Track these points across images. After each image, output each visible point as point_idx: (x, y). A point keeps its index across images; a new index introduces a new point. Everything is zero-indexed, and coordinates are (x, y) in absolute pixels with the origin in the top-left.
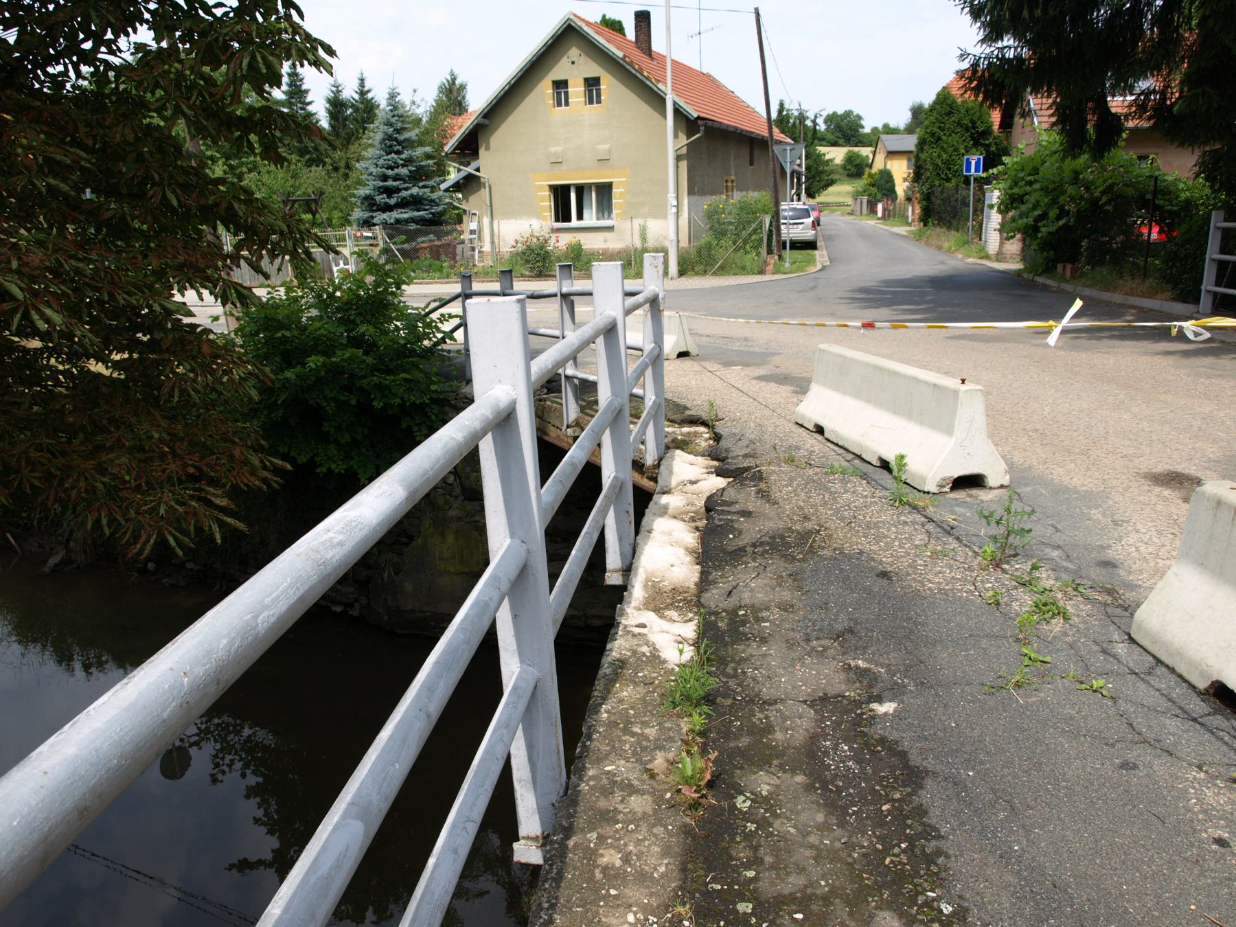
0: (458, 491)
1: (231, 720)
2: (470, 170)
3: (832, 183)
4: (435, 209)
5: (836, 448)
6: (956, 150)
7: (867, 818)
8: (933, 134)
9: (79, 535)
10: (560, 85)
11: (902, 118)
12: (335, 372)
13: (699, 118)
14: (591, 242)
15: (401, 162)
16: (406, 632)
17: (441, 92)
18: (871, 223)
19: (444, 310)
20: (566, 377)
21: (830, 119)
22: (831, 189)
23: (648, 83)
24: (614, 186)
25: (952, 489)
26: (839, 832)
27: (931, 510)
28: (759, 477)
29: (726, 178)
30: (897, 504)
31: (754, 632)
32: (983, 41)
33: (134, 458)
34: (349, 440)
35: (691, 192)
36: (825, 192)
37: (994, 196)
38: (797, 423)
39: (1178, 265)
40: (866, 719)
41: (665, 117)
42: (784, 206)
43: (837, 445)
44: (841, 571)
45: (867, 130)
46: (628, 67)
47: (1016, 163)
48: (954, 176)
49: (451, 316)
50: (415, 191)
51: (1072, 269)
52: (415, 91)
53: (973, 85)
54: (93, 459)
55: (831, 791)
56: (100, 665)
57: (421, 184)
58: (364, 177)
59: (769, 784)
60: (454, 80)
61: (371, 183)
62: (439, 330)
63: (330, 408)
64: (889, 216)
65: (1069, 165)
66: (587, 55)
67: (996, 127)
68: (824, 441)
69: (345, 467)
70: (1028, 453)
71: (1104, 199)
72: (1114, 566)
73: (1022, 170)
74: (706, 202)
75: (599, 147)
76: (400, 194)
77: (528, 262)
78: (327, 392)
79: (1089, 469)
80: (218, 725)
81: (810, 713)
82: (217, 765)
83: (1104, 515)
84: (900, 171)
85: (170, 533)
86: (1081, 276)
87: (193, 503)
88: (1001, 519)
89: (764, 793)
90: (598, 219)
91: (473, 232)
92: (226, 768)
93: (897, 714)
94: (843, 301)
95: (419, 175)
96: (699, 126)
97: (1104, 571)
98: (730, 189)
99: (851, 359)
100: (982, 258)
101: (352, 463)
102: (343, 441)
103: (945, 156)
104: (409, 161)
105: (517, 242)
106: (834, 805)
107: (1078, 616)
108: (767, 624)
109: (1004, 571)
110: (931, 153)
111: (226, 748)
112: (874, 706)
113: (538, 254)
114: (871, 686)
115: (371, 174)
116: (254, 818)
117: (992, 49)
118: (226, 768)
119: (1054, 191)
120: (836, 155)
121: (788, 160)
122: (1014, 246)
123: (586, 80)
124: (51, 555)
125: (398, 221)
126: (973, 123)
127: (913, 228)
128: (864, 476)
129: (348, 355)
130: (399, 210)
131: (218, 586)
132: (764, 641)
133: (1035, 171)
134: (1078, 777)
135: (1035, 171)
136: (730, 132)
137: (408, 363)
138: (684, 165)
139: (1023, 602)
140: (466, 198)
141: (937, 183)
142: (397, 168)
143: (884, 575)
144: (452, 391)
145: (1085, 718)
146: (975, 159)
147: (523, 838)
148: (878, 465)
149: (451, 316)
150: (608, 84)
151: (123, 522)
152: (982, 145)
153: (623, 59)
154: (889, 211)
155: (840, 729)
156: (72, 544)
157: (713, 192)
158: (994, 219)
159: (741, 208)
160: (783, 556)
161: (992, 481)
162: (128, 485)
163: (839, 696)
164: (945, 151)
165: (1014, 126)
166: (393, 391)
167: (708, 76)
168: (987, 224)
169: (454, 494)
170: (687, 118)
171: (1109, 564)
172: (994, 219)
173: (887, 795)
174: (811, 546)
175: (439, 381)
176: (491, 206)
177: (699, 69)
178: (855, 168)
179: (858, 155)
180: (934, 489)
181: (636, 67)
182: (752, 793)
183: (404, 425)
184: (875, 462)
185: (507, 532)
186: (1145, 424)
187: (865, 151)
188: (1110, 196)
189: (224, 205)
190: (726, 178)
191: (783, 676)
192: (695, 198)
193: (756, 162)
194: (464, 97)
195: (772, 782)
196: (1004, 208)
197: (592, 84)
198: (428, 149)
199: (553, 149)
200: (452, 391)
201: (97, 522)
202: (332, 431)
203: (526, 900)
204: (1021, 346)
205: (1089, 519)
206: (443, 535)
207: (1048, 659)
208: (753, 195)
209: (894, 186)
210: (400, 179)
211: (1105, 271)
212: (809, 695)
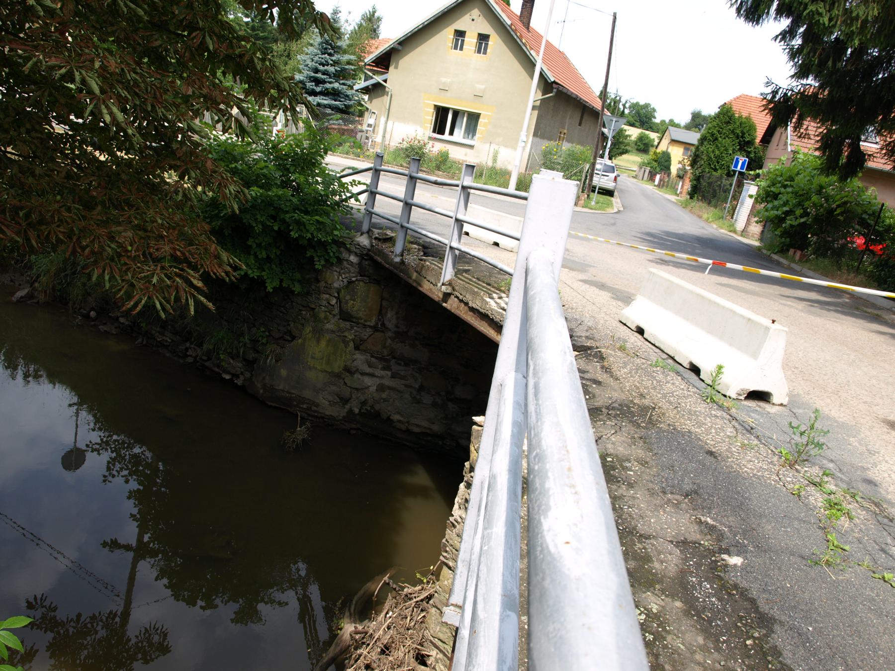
0: (336, 311)
1: (126, 438)
2: (378, 79)
3: (625, 152)
4: (347, 102)
5: (654, 348)
6: (726, 150)
7: (735, 647)
8: (713, 135)
9: (43, 279)
10: (460, 34)
11: (684, 118)
12: (269, 203)
13: (554, 82)
14: (456, 154)
15: (331, 62)
16: (274, 405)
17: (363, 19)
18: (649, 187)
19: (356, 177)
20: (451, 248)
21: (634, 106)
22: (625, 156)
23: (524, 48)
24: (481, 116)
25: (746, 398)
26: (716, 655)
27: (733, 411)
28: (602, 358)
29: (561, 130)
30: (708, 401)
31: (622, 476)
32: (792, 77)
33: (137, 234)
34: (265, 256)
35: (535, 134)
36: (620, 158)
37: (751, 189)
38: (621, 322)
39: (886, 270)
40: (721, 566)
41: (532, 76)
42: (599, 160)
43: (654, 345)
44: (679, 443)
45: (657, 120)
46: (512, 33)
47: (777, 170)
48: (720, 168)
49: (359, 183)
50: (336, 85)
51: (801, 255)
52: (350, 13)
53: (770, 107)
54: (106, 228)
55: (703, 619)
56: (37, 377)
57: (342, 82)
58: (301, 67)
59: (656, 604)
60: (374, 12)
61: (306, 72)
62: (348, 191)
63: (258, 228)
64: (663, 186)
65: (823, 179)
66: (484, 17)
67: (758, 140)
68: (643, 340)
69: (258, 274)
70: (794, 384)
71: (838, 211)
72: (876, 485)
73: (781, 176)
74: (545, 144)
75: (478, 86)
76: (325, 85)
77: (408, 156)
78: (258, 217)
79: (841, 406)
80: (115, 441)
81: (676, 551)
82: (109, 469)
83: (860, 444)
84: (678, 157)
85: (157, 297)
86: (807, 261)
87: (178, 279)
88: (804, 432)
89: (655, 611)
90: (464, 138)
91: (370, 126)
92: (116, 473)
93: (744, 568)
94: (636, 239)
95: (342, 75)
96: (553, 88)
97: (869, 487)
98: (561, 139)
99: (677, 285)
100: (730, 231)
101: (264, 273)
102: (260, 257)
103: (717, 152)
104: (336, 63)
105: (403, 140)
106: (706, 629)
107: (858, 518)
108: (632, 473)
109: (797, 471)
110: (708, 147)
111: (119, 458)
112: (725, 557)
113: (417, 153)
114: (719, 541)
115: (307, 65)
116: (131, 514)
117: (798, 84)
118: (116, 473)
119: (802, 197)
120: (633, 133)
121: (612, 128)
122: (756, 229)
123: (480, 35)
124: (19, 289)
125: (319, 105)
126: (743, 133)
127: (679, 198)
128: (678, 373)
129: (281, 193)
130: (322, 97)
131: (140, 340)
132: (631, 486)
133: (791, 179)
134: (890, 650)
135: (791, 179)
136: (572, 98)
137: (322, 209)
138: (536, 112)
139: (817, 499)
140: (370, 99)
141: (707, 170)
142: (327, 65)
143: (711, 453)
144: (349, 238)
145: (884, 601)
146: (742, 160)
147: (452, 605)
148: (688, 367)
149: (359, 183)
150: (495, 42)
151: (120, 282)
152: (745, 150)
153: (510, 27)
154: (664, 182)
155: (701, 570)
156: (36, 285)
157: (550, 139)
158: (746, 205)
159: (569, 155)
160: (631, 422)
161: (775, 399)
162: (129, 254)
163: (697, 543)
164: (718, 149)
165: (771, 143)
166: (307, 227)
167: (562, 53)
168: (740, 208)
169: (334, 313)
170: (546, 79)
171: (869, 482)
172: (746, 205)
173: (747, 632)
174: (650, 418)
175: (341, 229)
176: (389, 110)
177: (557, 47)
178: (643, 146)
179: (647, 137)
180: (734, 396)
181: (518, 34)
182: (645, 609)
183: (309, 254)
184: (686, 365)
185: (514, 367)
186: (874, 381)
187: (653, 136)
188: (843, 209)
189: (247, 58)
190: (561, 130)
191: (652, 517)
192: (537, 139)
193: (583, 124)
194: (378, 27)
195: (658, 603)
196: (759, 199)
197: (483, 38)
198: (353, 57)
199: (443, 80)
200: (349, 238)
201: (101, 276)
202: (254, 246)
203: (335, 621)
204: (772, 302)
205: (849, 444)
206: (318, 341)
207: (847, 548)
208: (578, 148)
209: (670, 165)
210: (327, 74)
211: (826, 261)
212: (673, 537)
